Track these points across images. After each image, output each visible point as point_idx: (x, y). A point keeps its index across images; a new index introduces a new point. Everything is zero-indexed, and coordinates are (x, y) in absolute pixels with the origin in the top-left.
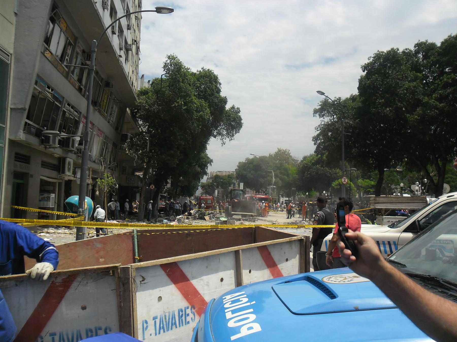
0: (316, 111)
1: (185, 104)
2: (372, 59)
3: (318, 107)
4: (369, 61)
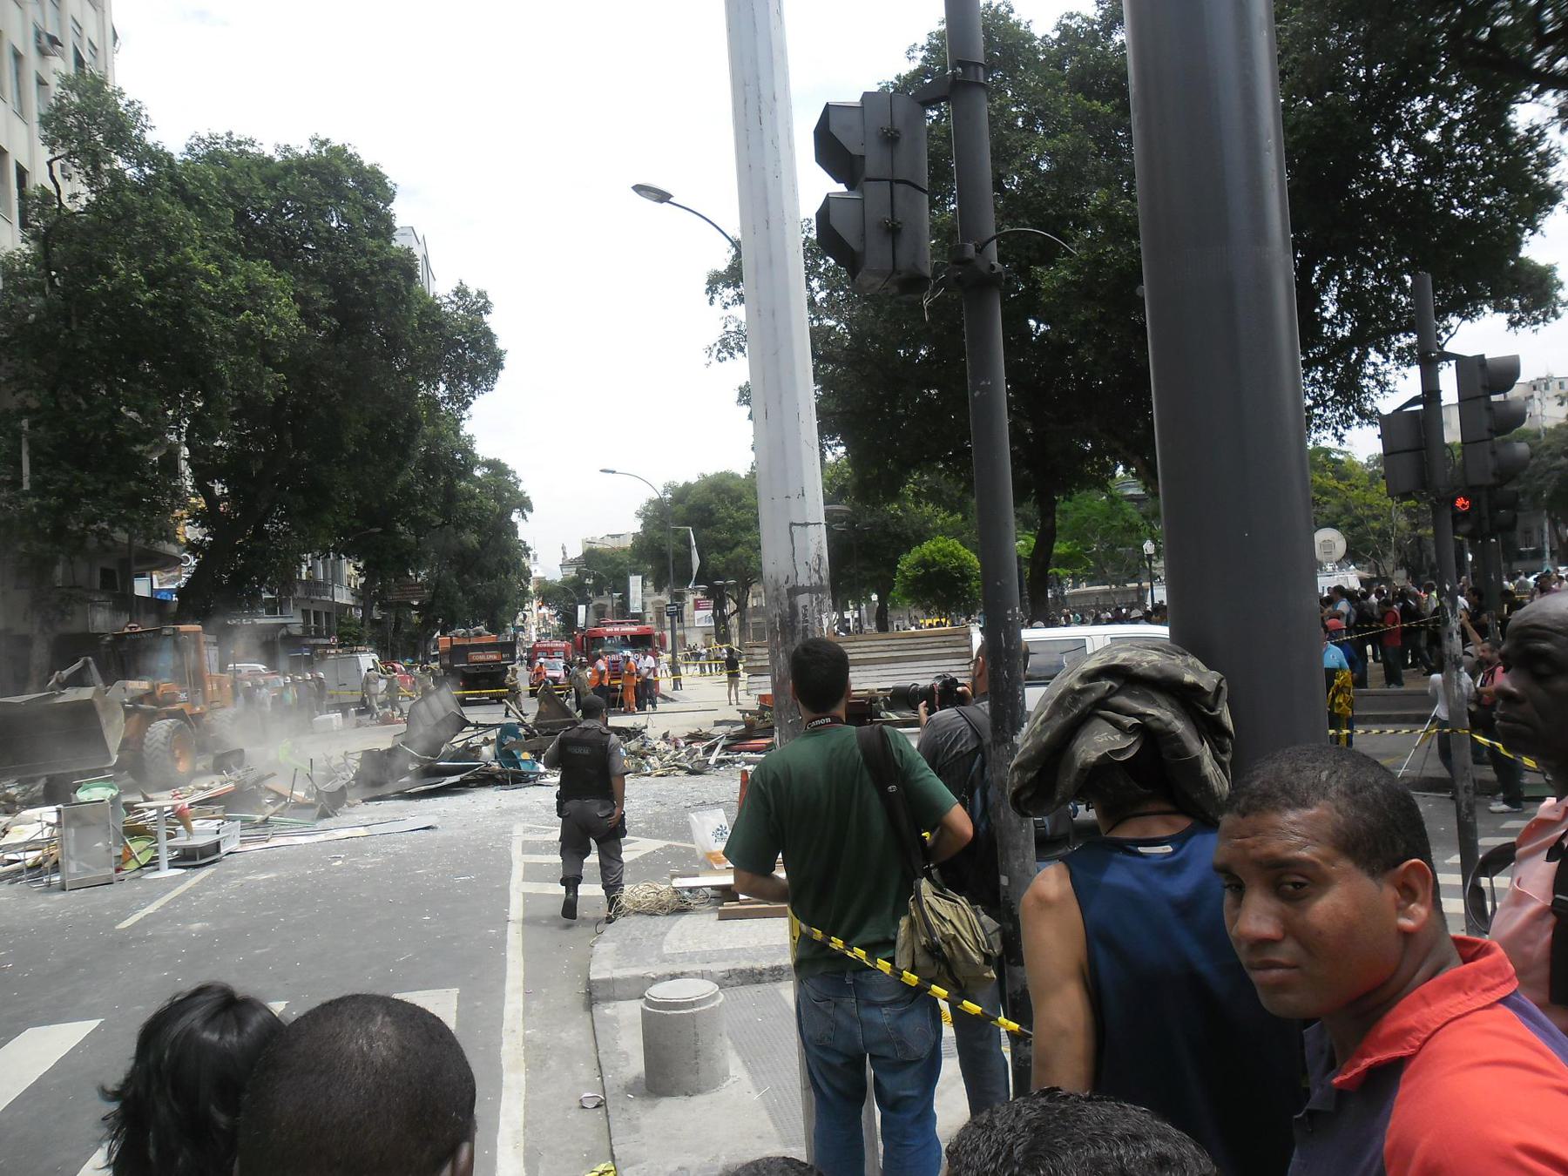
4: (915, 65)
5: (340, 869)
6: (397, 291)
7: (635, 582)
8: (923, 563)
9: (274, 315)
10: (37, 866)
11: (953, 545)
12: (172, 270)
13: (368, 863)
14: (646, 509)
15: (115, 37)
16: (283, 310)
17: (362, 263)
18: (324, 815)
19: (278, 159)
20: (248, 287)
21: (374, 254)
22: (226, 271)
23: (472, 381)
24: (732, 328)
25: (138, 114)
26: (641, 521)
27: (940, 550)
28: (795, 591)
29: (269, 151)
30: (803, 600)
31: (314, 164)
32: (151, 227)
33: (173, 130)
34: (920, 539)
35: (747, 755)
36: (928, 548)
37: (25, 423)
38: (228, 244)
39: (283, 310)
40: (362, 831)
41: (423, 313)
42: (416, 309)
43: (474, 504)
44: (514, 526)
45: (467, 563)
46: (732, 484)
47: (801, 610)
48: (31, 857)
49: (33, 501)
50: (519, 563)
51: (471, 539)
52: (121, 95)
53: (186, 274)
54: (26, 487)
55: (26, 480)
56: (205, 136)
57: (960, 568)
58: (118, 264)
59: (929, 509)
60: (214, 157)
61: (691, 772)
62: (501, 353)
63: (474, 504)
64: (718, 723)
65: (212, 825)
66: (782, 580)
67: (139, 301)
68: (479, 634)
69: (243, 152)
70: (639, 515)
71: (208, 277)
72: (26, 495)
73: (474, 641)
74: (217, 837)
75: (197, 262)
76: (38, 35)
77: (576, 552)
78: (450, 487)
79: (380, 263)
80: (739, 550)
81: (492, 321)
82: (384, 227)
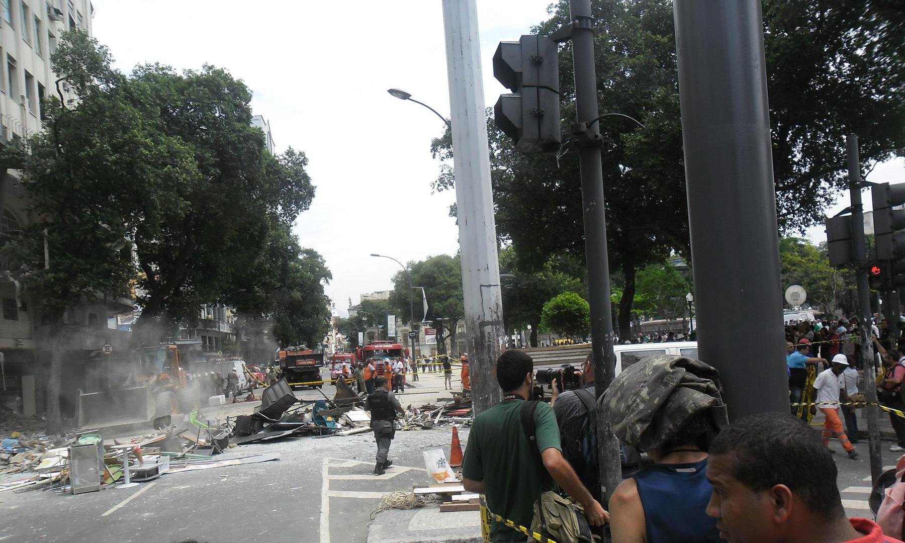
0: (436, 145)
1: (116, 149)
2: (555, 10)
3: (440, 136)
4: (552, 16)
5: (225, 483)
6: (253, 153)
7: (391, 319)
8: (557, 307)
9: (184, 168)
10: (57, 481)
11: (575, 296)
12: (126, 143)
13: (241, 479)
14: (397, 277)
15: (92, 9)
16: (189, 165)
17: (233, 137)
18: (215, 453)
19: (185, 77)
20: (169, 152)
21: (240, 131)
22: (157, 142)
23: (297, 204)
24: (446, 171)
25: (105, 53)
26: (394, 284)
27: (567, 299)
28: (483, 324)
29: (179, 73)
30: (488, 329)
31: (206, 80)
32: (114, 118)
33: (125, 61)
34: (556, 293)
35: (456, 418)
36: (560, 298)
37: (46, 231)
38: (158, 127)
39: (189, 165)
40: (238, 462)
41: (268, 165)
42: (265, 163)
43: (298, 275)
44: (322, 287)
45: (295, 309)
46: (446, 262)
47: (487, 335)
48: (54, 476)
49: (51, 275)
50: (324, 309)
51: (297, 295)
52: (96, 42)
53: (134, 145)
54: (47, 267)
55: (47, 263)
56: (143, 65)
57: (579, 310)
58: (96, 140)
59: (561, 276)
60: (148, 77)
61: (424, 428)
62: (313, 188)
63: (298, 275)
64: (439, 400)
65: (154, 458)
66: (476, 319)
67: (108, 161)
68: (302, 350)
69: (165, 74)
70: (393, 280)
71: (146, 147)
72: (47, 272)
73: (299, 354)
74: (155, 465)
75: (140, 138)
76: (49, 9)
77: (357, 302)
78: (285, 264)
79: (244, 137)
80: (451, 300)
81: (308, 169)
82: (246, 116)
